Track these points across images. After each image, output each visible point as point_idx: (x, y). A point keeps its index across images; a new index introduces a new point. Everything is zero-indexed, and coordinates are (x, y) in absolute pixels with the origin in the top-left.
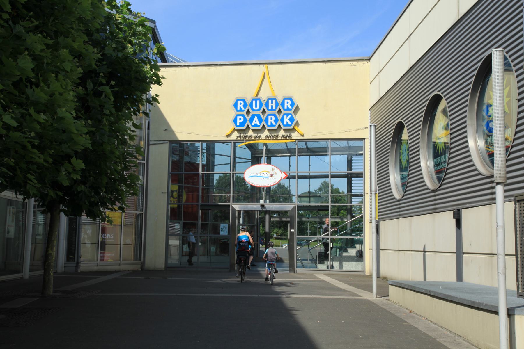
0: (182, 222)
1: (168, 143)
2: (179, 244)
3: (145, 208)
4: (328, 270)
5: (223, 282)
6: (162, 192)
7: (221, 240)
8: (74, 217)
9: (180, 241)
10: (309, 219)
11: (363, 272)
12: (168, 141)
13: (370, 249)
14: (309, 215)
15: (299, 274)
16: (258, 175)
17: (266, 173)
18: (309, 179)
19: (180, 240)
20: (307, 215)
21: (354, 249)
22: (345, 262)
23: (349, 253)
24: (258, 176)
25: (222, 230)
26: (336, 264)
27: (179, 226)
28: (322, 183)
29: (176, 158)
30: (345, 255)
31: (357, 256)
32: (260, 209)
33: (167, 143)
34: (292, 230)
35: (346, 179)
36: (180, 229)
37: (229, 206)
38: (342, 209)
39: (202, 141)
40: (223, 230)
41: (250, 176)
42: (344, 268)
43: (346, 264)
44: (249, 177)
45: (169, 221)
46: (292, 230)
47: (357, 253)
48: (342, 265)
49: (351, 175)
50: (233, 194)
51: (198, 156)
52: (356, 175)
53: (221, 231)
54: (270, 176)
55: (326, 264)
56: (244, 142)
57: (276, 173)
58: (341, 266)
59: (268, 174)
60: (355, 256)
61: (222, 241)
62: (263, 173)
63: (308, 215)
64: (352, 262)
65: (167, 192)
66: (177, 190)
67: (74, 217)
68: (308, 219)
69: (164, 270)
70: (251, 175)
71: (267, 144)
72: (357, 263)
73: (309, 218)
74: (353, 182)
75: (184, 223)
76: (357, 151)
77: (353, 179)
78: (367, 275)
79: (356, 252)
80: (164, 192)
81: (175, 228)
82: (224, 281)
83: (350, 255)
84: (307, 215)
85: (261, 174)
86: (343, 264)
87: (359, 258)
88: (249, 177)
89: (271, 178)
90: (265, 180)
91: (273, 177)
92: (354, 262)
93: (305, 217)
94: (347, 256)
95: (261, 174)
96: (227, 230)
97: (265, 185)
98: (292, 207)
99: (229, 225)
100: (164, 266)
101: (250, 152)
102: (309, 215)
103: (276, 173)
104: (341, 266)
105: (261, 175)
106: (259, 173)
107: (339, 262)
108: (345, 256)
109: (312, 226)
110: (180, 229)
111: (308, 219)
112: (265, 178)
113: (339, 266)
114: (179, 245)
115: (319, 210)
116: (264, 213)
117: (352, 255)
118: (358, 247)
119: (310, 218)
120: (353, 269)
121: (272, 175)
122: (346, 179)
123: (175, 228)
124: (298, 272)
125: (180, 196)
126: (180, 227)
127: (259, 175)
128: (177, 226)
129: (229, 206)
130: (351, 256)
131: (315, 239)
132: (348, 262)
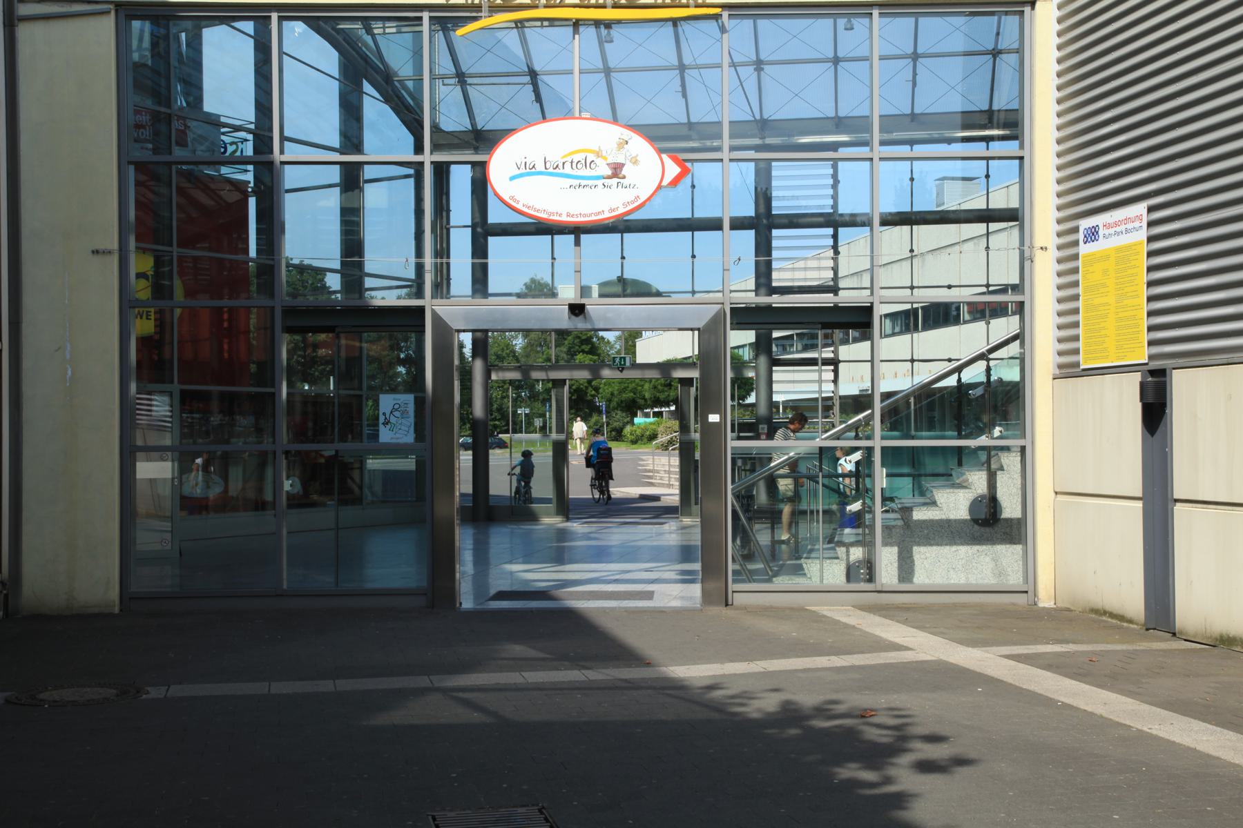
0: (176, 387)
1: (113, 13)
2: (170, 476)
3: (10, 323)
4: (853, 586)
5: (476, 717)
6: (95, 248)
7: (323, 453)
8: (332, 388)
9: (176, 465)
10: (624, 372)
11: (1026, 592)
12: (111, 7)
13: (1056, 493)
14: (624, 358)
15: (745, 609)
16: (551, 170)
17: (591, 157)
18: (620, 235)
19: (173, 461)
20: (618, 360)
21: (962, 491)
22: (923, 549)
23: (941, 509)
24: (551, 174)
25: (386, 423)
26: (887, 559)
27: (168, 408)
28: (525, 284)
29: (144, 153)
30: (925, 518)
31: (975, 521)
32: (563, 320)
33: (107, 12)
34: (714, 418)
35: (753, 232)
36: (171, 417)
37: (421, 310)
38: (580, 350)
39: (278, 11)
40: (393, 420)
41: (518, 172)
42: (921, 578)
43: (928, 555)
44: (512, 178)
45: (133, 387)
46: (714, 418)
47: (975, 505)
48: (913, 561)
49: (771, 220)
50: (436, 257)
51: (222, 150)
52: (785, 221)
53: (381, 427)
54: (609, 172)
55: (844, 556)
56: (483, 14)
57: (635, 162)
58: (906, 567)
59: (599, 161)
60: (964, 521)
61: (322, 456)
62: (576, 158)
63: (621, 358)
64: (954, 548)
65: (121, 250)
66: (150, 273)
67: (332, 388)
68: (621, 371)
69: (116, 610)
70: (523, 171)
71: (357, 191)
72: (976, 548)
73: (623, 369)
74: (775, 243)
75: (183, 392)
76: (790, 136)
77: (775, 232)
78: (1046, 605)
79: (967, 504)
80: (101, 247)
81: (153, 413)
82: (468, 704)
83: (944, 517)
84: (618, 360)
85: (568, 165)
86: (916, 557)
87: (983, 529)
88: (512, 178)
89: (615, 180)
90: (587, 189)
91: (624, 177)
92: (961, 547)
93: (609, 366)
94: (932, 521)
95: (568, 165)
96: (412, 420)
97: (585, 215)
98: (716, 311)
99: (420, 403)
100: (114, 594)
101: (412, 138)
102: (624, 358)
103: (635, 162)
104: (906, 567)
105: (568, 170)
106: (555, 157)
107: (899, 547)
108: (924, 521)
109: (504, 394)
110: (171, 417)
111: (621, 371)
112: (583, 182)
113: (896, 565)
114: (173, 479)
115: (823, 328)
116: (377, 363)
117: (952, 517)
118: (977, 481)
119: (628, 368)
120: (958, 579)
121: (617, 170)
122: (753, 232)
123: (153, 413)
124: (739, 599)
125: (160, 290)
126: (171, 411)
127: (557, 171)
128: (161, 407)
129: (421, 310)
130: (949, 521)
131: (792, 454)
132: (935, 548)
